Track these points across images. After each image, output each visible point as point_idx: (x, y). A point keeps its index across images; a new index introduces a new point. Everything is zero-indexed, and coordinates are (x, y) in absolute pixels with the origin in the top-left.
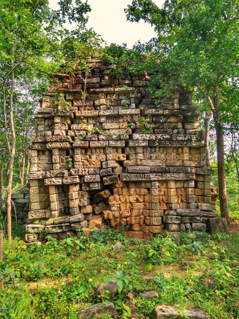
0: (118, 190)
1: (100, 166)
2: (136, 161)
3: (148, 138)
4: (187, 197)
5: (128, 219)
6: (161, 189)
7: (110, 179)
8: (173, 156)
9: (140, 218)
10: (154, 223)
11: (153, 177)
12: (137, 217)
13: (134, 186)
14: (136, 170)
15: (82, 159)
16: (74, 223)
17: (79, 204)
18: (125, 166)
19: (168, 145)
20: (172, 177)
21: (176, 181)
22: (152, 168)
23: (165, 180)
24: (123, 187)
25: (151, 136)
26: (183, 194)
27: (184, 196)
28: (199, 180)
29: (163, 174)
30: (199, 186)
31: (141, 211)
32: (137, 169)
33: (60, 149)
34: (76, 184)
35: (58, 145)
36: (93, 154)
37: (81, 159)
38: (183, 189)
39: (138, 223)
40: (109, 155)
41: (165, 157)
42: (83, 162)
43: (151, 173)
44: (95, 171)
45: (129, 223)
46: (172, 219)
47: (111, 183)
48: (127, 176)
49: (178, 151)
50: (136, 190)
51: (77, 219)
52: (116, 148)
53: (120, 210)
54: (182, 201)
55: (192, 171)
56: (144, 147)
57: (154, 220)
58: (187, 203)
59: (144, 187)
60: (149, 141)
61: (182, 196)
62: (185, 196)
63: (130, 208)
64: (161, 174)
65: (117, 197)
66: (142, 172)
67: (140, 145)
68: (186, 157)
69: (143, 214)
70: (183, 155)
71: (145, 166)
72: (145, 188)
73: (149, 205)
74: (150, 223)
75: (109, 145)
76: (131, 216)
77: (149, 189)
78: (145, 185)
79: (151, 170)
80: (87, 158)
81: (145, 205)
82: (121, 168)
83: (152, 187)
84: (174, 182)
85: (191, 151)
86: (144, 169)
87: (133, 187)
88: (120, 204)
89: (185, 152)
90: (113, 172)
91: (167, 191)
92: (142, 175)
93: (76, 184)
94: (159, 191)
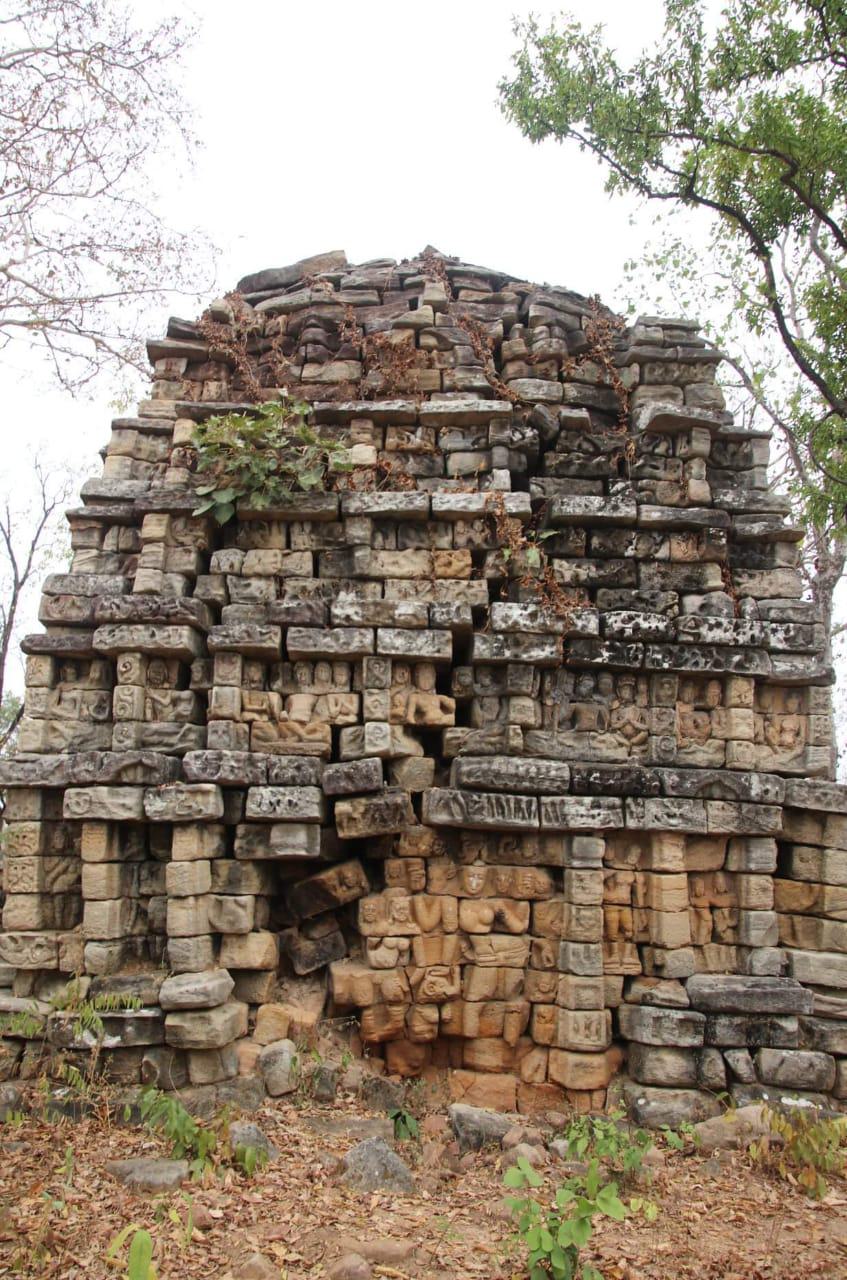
2: (504, 734)
5: (447, 1012)
6: (614, 876)
8: (683, 718)
11: (580, 812)
13: (485, 853)
14: (498, 775)
15: (248, 707)
16: (181, 1010)
21: (692, 839)
24: (433, 855)
27: (726, 912)
28: (798, 840)
29: (629, 800)
31: (515, 975)
32: (503, 770)
33: (149, 657)
35: (140, 636)
37: (243, 709)
38: (721, 879)
40: (371, 694)
42: (250, 723)
43: (571, 792)
45: (453, 1029)
48: (455, 799)
49: (701, 697)
50: (495, 873)
52: (409, 665)
54: (715, 937)
55: (766, 792)
56: (543, 668)
58: (740, 946)
62: (731, 914)
64: (617, 801)
66: (526, 784)
71: (543, 757)
72: (538, 866)
73: (554, 952)
77: (557, 873)
78: (543, 850)
79: (572, 778)
82: (431, 762)
84: (682, 843)
85: (767, 700)
90: (388, 776)
91: (647, 884)
92: (524, 798)
94: (605, 882)
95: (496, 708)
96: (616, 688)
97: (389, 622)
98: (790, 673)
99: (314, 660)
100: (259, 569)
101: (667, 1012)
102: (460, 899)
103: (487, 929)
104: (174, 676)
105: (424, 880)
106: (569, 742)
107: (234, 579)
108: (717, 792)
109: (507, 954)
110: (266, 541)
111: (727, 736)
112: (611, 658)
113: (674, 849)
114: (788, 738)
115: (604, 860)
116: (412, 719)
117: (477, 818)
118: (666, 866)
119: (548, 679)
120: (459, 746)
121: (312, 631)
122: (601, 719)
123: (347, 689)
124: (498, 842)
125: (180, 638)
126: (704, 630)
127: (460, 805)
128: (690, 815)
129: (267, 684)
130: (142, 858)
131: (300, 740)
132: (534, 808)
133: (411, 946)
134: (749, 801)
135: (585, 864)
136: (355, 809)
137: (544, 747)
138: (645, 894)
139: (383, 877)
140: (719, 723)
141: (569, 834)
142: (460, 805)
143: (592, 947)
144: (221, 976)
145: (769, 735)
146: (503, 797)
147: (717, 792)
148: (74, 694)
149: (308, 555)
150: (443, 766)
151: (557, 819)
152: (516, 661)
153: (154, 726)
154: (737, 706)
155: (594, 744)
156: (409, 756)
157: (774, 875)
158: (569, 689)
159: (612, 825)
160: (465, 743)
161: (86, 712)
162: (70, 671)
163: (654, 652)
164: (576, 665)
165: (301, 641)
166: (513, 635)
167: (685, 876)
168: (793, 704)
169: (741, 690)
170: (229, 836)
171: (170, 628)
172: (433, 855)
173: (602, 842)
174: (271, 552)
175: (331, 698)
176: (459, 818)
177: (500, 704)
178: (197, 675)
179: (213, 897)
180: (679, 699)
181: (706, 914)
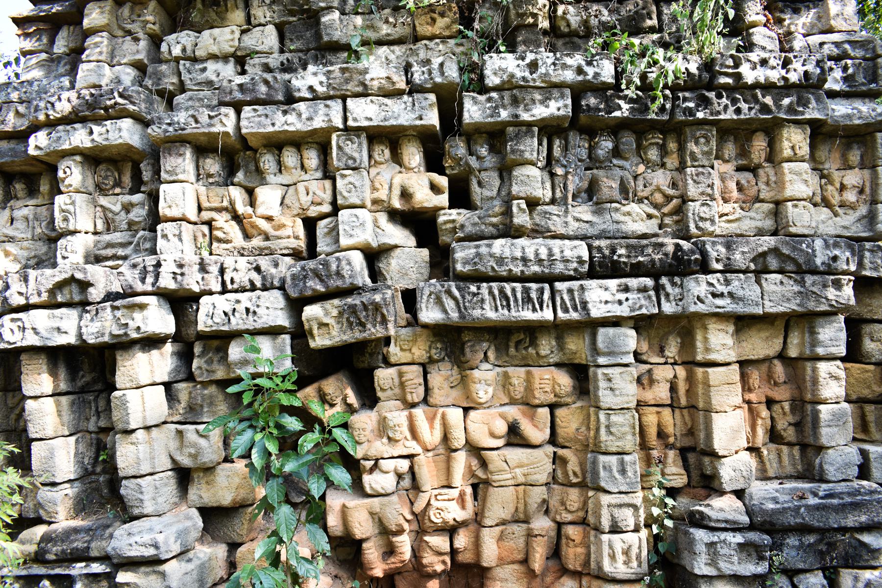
0: (401, 375)
1: (302, 244)
2: (508, 212)
3: (569, 76)
4: (803, 417)
5: (462, 540)
6: (649, 371)
7: (341, 314)
8: (723, 180)
9: (530, 535)
10: (603, 484)
11: (602, 297)
12: (515, 527)
13: (491, 355)
14: (501, 260)
15: (205, 204)
16: (133, 564)
17: (179, 458)
18: (444, 238)
19: (690, 112)
20: (722, 295)
21: (743, 323)
22: (599, 249)
23: (674, 318)
24: (431, 361)
25: (589, 63)
26: (782, 394)
27: (787, 406)
28: (868, 316)
29: (664, 280)
30: (869, 346)
31: (538, 494)
32: (507, 253)
33: (93, 159)
34: (152, 342)
35: (80, 137)
36: (263, 182)
37: (200, 209)
38: (779, 369)
39: (520, 557)
40: (343, 176)
41: (674, 185)
42: (209, 223)
43: (592, 274)
44: (258, 269)
45: (466, 557)
46: (716, 553)
47: (348, 337)
48: (449, 292)
49: (744, 153)
50: (506, 376)
51: (144, 545)
52: (387, 138)
53: (416, 487)
54: (774, 436)
55: (835, 258)
56: (549, 130)
57: (606, 550)
58: (804, 447)
59: (553, 359)
60: (578, 91)
61: (776, 407)
62: (793, 409)
63: (474, 475)
64: (649, 282)
65: (398, 417)
66: (536, 269)
67: (525, 117)
68: (799, 180)
69: (547, 512)
70: (779, 173)
71: (554, 237)
72: (557, 365)
73: (582, 465)
74: (587, 563)
75: (345, 119)
76: (478, 520)
77: (581, 374)
78: (561, 347)
79: (591, 257)
80: (232, 203)
81: (556, 458)
82: (425, 252)
83: (601, 360)
84: (731, 328)
85: (822, 154)
86: (550, 254)
87: (486, 359)
88: (411, 457)
89: (787, 152)
90: (375, 274)
91: (690, 379)
92: (534, 286)
93: (152, 342)
94: (639, 380)
95: (497, 183)
96: (640, 149)
97: (360, 89)
98: (849, 116)
99: (278, 144)
100: (214, 49)
101: (723, 535)
102: (466, 410)
103: (500, 443)
104: (127, 179)
105: (421, 390)
106: (588, 217)
107: (188, 64)
108: (773, 263)
109: (525, 470)
110: (223, 19)
111: (779, 197)
112: (632, 110)
113: (722, 335)
114: (851, 196)
115: (636, 354)
116: (397, 204)
117: (477, 313)
118: (713, 357)
119: (557, 142)
120: (454, 230)
121: (269, 109)
122: (624, 189)
123: (319, 174)
124: (508, 340)
125: (124, 133)
126: (745, 69)
127: (454, 299)
128: (740, 293)
129: (228, 180)
130: (99, 386)
131: (267, 238)
132: (546, 296)
133: (411, 468)
134: (814, 272)
135: (613, 361)
136: (327, 313)
137: (556, 225)
138: (687, 391)
139: (374, 390)
140: (767, 184)
141: (592, 326)
142: (454, 299)
143: (627, 458)
144: (188, 518)
145: (828, 194)
146: (508, 287)
147: (773, 263)
148: (25, 211)
149: (271, 28)
150: (441, 264)
151: (575, 309)
152: (516, 122)
153: (107, 238)
154: (789, 160)
155: (617, 216)
156: (396, 247)
157: (843, 359)
158: (584, 154)
159: (644, 311)
160: (462, 226)
161: (38, 230)
162: (19, 187)
163: (685, 99)
164: (590, 125)
165: (256, 122)
166: (513, 90)
167: (736, 367)
168: (855, 156)
169: (795, 139)
170: (185, 356)
171: (108, 123)
172: (431, 361)
173: (633, 333)
174: (227, 30)
175: (301, 187)
176: (454, 315)
177: (501, 177)
178: (146, 175)
179: (173, 427)
180: (717, 158)
181: (765, 413)
